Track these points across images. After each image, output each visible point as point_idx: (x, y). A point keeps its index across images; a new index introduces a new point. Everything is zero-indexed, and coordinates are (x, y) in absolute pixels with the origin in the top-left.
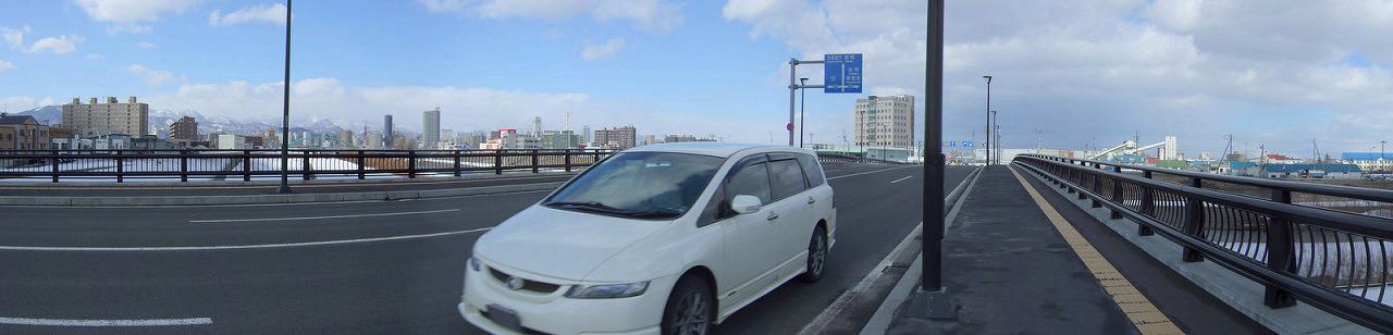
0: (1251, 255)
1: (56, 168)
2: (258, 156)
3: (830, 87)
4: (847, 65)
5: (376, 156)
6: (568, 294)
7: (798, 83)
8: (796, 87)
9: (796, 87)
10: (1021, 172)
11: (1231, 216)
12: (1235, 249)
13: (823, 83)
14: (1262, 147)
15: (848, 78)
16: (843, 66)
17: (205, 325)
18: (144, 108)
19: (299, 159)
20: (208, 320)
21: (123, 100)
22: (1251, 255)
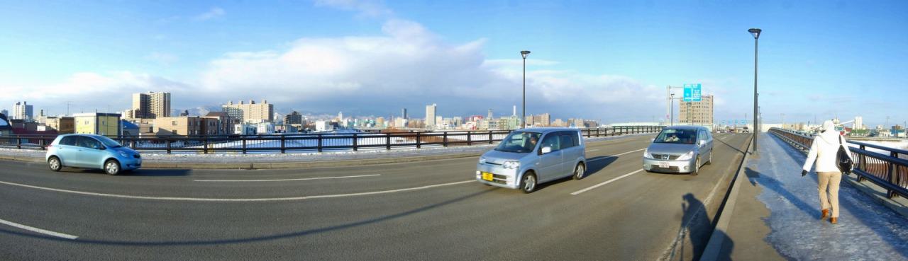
4: (694, 89)
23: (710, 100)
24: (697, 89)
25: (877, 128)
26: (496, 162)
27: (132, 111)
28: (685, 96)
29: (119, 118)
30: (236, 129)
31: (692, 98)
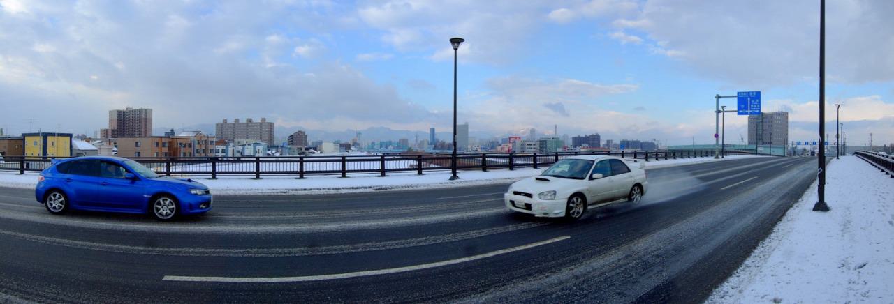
3: (741, 111)
4: (752, 98)
6: (52, 299)
7: (720, 109)
8: (720, 112)
9: (720, 112)
13: (736, 109)
15: (752, 106)
16: (749, 99)
18: (271, 125)
20: (167, 278)
21: (257, 120)
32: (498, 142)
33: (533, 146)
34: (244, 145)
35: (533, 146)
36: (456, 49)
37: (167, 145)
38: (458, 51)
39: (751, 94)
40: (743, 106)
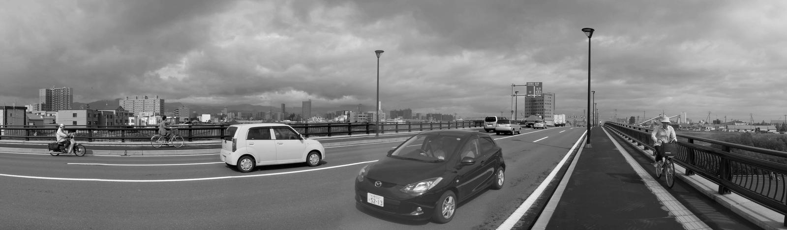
0: (743, 185)
1: (123, 135)
2: (197, 129)
4: (536, 87)
5: (315, 127)
10: (606, 129)
11: (706, 157)
12: (738, 183)
14: (725, 117)
17: (442, 181)
19: (186, 131)
20: (441, 179)
22: (743, 185)
23: (552, 97)
24: (538, 87)
25: (700, 122)
26: (710, 144)
27: (38, 105)
28: (528, 93)
29: (25, 111)
30: (130, 121)
31: (534, 95)
32: (334, 114)
33: (363, 118)
34: (148, 117)
35: (363, 118)
36: (378, 57)
37: (97, 116)
38: (379, 58)
39: (536, 84)
40: (530, 92)
